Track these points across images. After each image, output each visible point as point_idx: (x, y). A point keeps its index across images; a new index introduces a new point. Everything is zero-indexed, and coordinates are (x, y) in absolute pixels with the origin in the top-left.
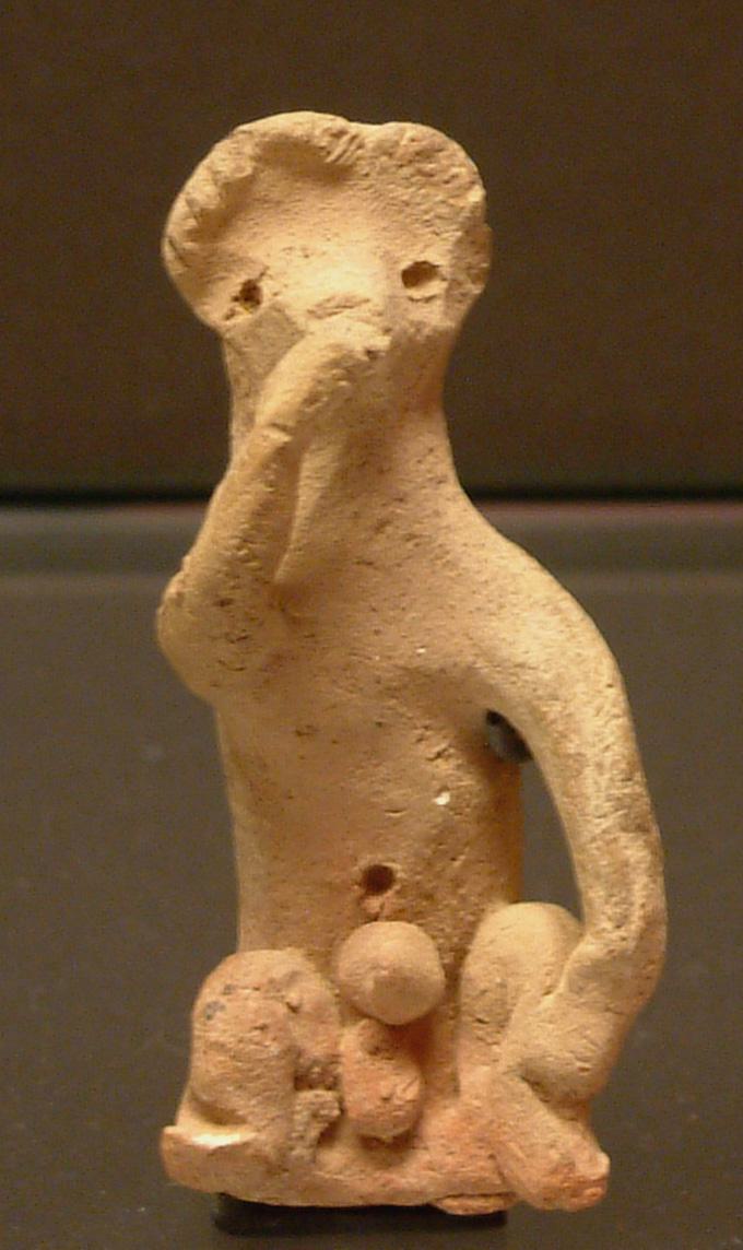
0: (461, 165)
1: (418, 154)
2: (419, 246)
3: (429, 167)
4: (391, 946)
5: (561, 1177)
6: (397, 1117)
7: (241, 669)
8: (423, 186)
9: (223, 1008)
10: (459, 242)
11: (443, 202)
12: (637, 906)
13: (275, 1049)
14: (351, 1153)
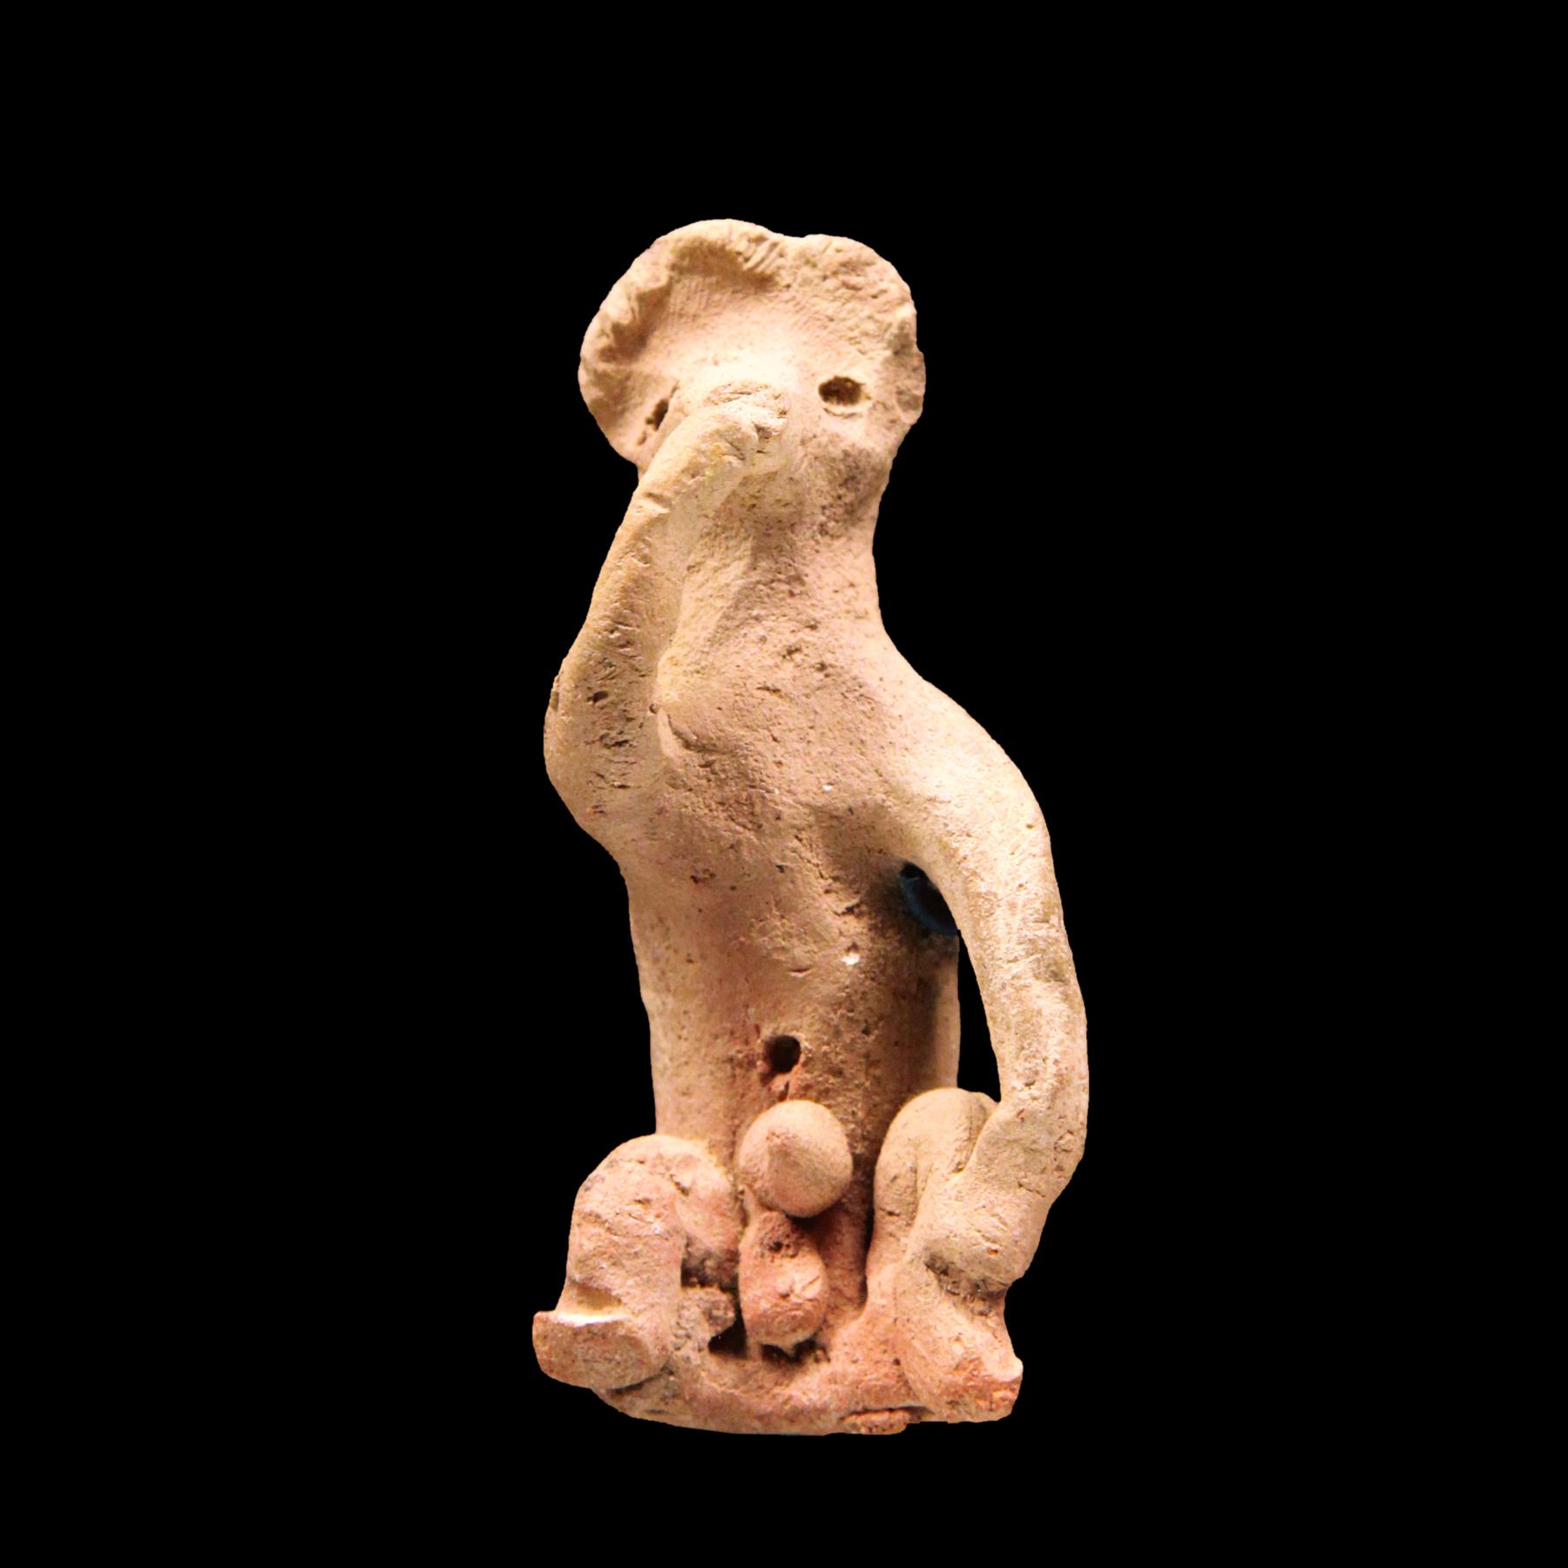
1: (844, 265)
2: (844, 364)
3: (854, 280)
5: (965, 1374)
6: (794, 1317)
7: (622, 787)
8: (848, 301)
10: (887, 361)
11: (870, 317)
12: (1050, 1062)
13: (658, 1227)
14: (760, 1363)
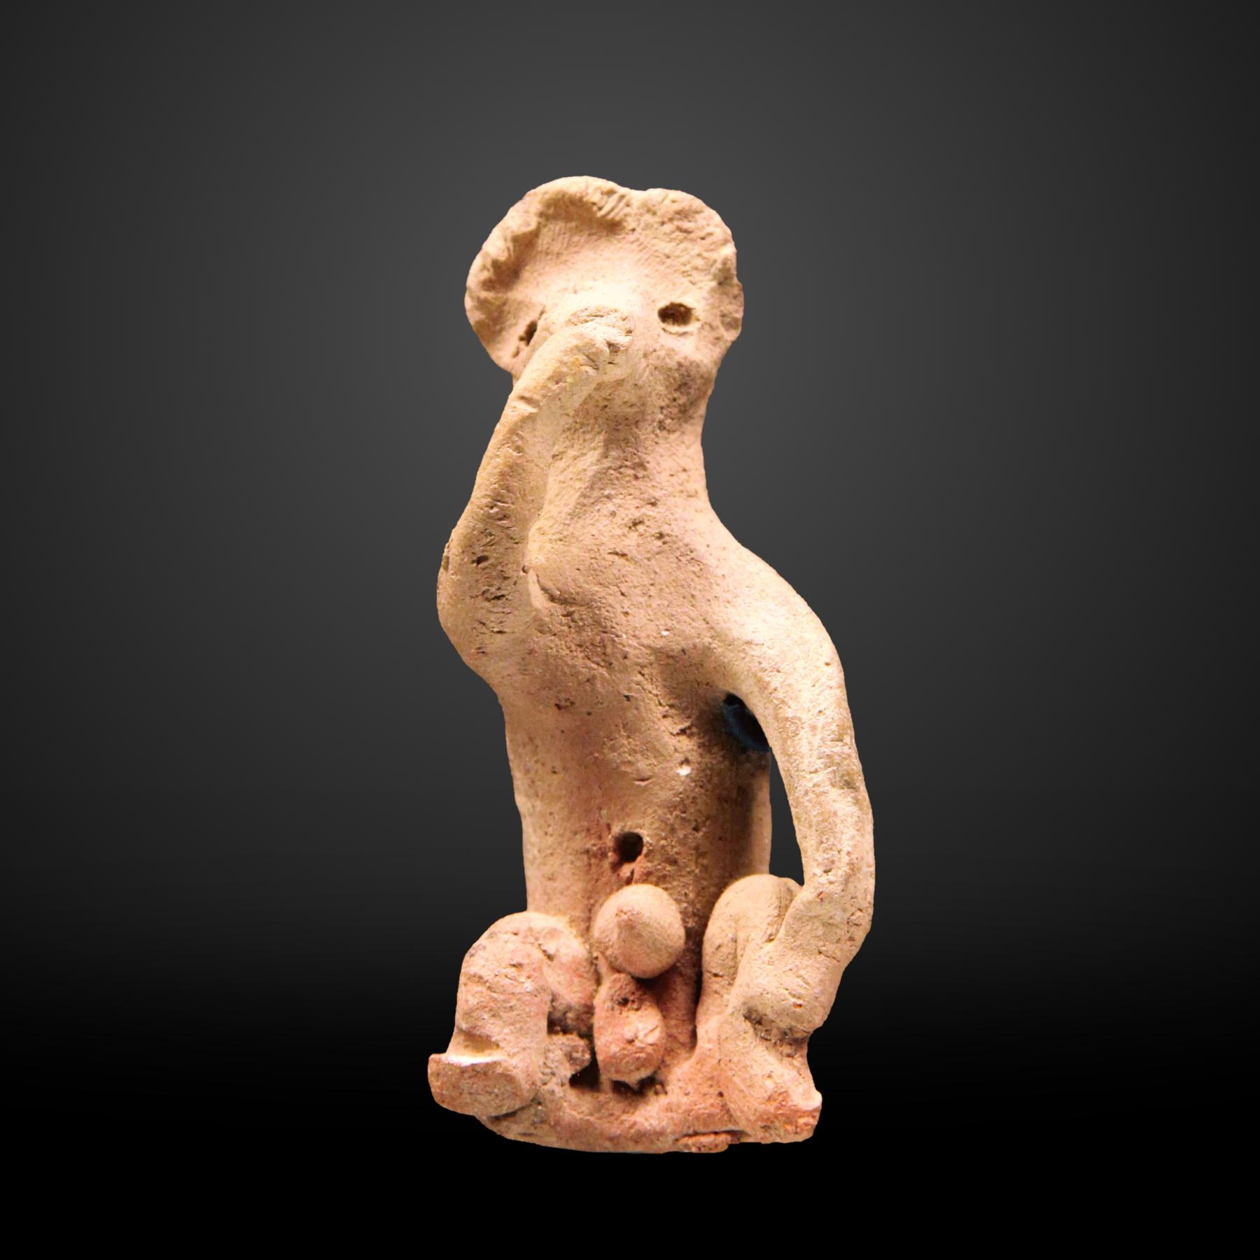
0: (717, 226)
1: (678, 213)
2: (678, 293)
3: (686, 225)
4: (650, 906)
5: (775, 1104)
6: (638, 1059)
7: (500, 632)
8: (681, 242)
10: (713, 290)
11: (699, 255)
12: (844, 854)
13: (529, 986)
14: (610, 1095)
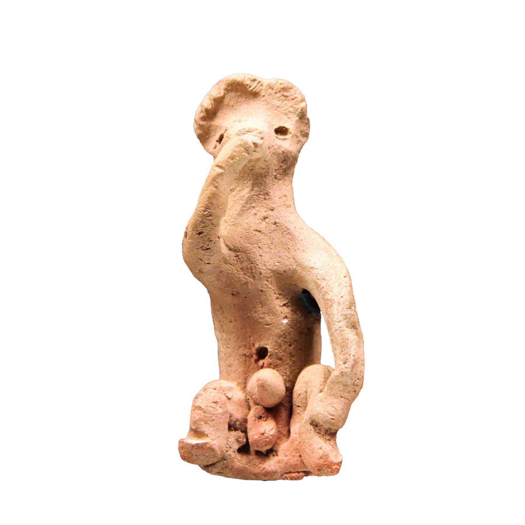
1: (283, 89)
2: (283, 122)
3: (286, 94)
5: (323, 460)
6: (266, 441)
7: (208, 263)
8: (284, 101)
9: (202, 395)
10: (297, 121)
11: (291, 106)
12: (351, 356)
13: (220, 411)
14: (254, 456)
